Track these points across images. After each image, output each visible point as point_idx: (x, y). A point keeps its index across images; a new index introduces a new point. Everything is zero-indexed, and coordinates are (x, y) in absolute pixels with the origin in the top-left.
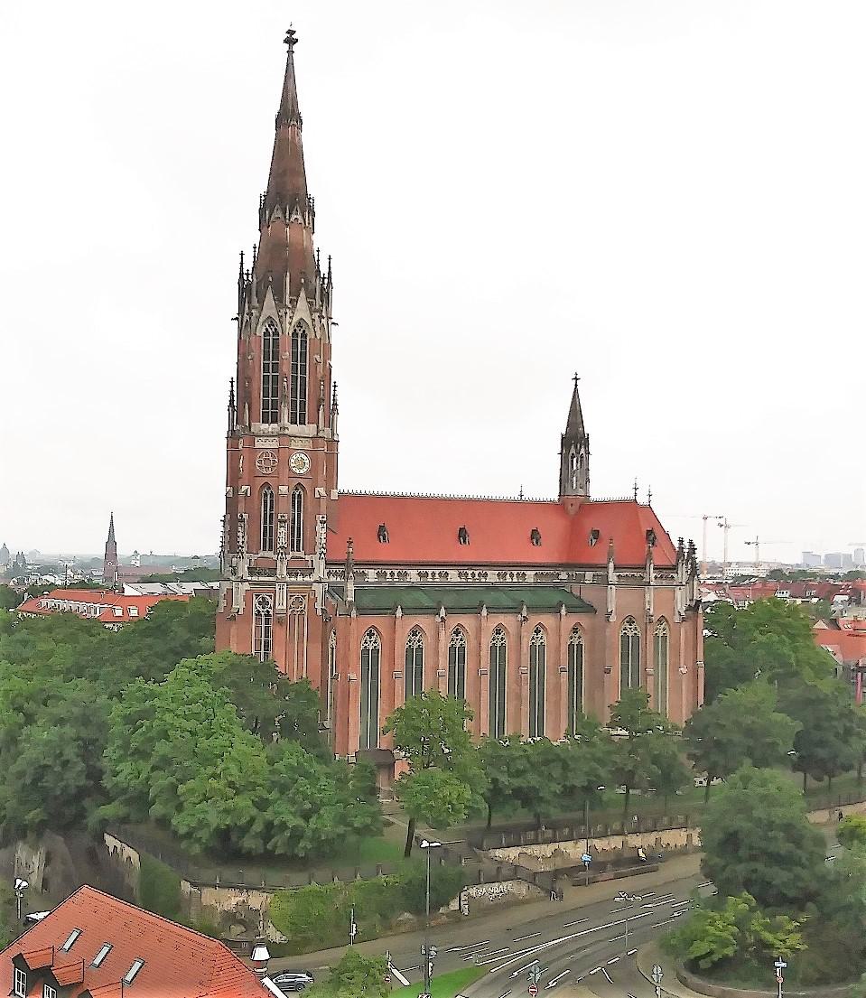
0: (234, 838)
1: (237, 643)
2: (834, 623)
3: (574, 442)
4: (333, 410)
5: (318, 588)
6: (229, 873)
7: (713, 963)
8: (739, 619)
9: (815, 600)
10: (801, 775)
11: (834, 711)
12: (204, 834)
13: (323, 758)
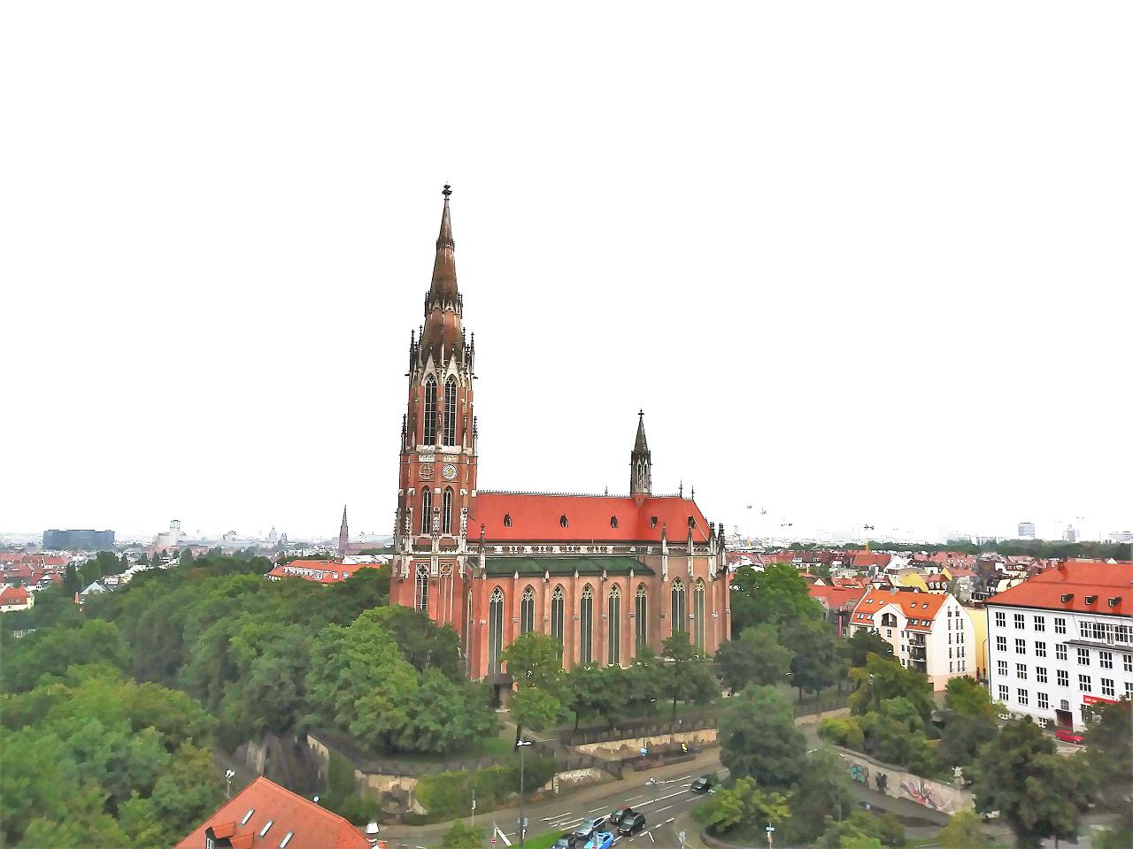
0: (393, 738)
1: (406, 599)
2: (828, 581)
3: (641, 455)
4: (474, 435)
5: (461, 559)
6: (388, 764)
7: (727, 827)
8: (758, 579)
9: (819, 565)
10: (797, 689)
11: (819, 643)
12: (372, 736)
13: (459, 680)
